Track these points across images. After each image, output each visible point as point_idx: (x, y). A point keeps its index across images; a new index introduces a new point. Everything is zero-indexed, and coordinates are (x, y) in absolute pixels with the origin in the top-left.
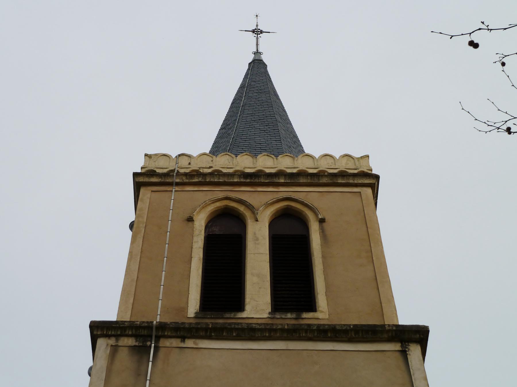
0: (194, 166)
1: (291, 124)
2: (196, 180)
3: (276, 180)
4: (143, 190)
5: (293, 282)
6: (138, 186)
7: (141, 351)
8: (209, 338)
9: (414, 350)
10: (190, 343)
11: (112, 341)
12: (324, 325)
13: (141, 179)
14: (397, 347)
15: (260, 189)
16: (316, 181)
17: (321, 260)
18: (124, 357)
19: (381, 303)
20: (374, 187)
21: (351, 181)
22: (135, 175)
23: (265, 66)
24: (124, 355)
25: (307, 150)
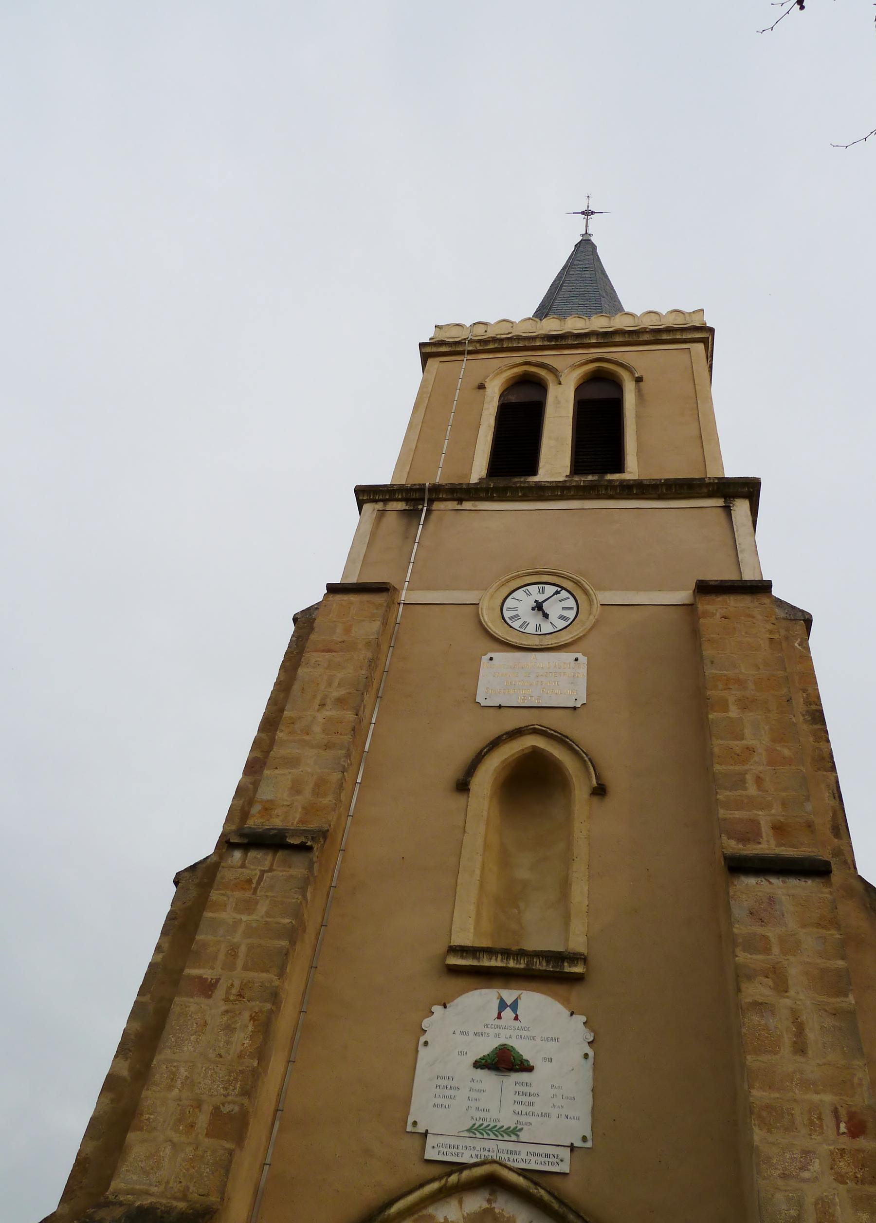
0: (491, 333)
1: (620, 303)
2: (491, 346)
6: (425, 358)
7: (411, 515)
8: (491, 499)
9: (741, 507)
10: (467, 505)
12: (630, 480)
13: (428, 350)
14: (720, 502)
17: (634, 420)
18: (392, 521)
19: (705, 461)
21: (678, 337)
22: (422, 345)
23: (594, 247)
25: (627, 309)
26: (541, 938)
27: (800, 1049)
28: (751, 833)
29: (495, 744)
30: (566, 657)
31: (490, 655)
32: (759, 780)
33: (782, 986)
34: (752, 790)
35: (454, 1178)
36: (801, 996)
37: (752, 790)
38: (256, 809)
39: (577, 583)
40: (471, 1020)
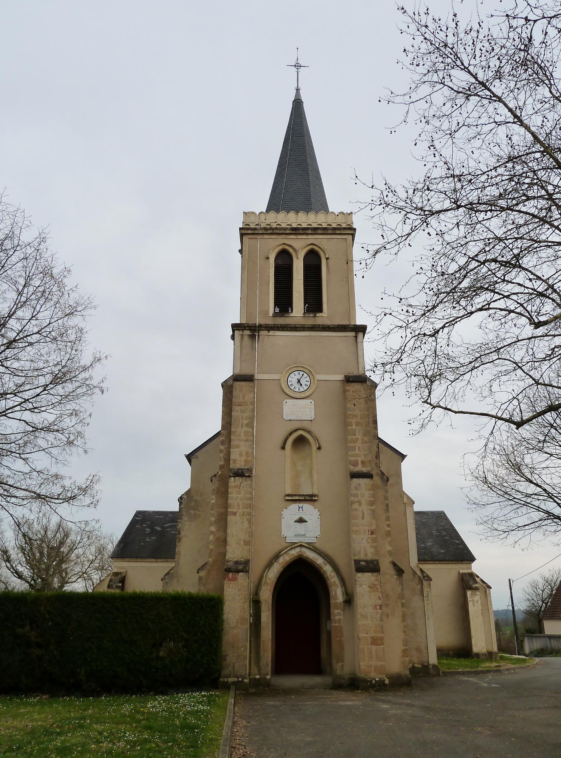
2: (269, 232)
3: (307, 232)
4: (244, 237)
5: (314, 303)
6: (242, 235)
10: (271, 333)
11: (241, 332)
13: (243, 232)
15: (299, 237)
16: (326, 232)
18: (246, 339)
20: (353, 235)
21: (343, 232)
22: (240, 229)
24: (246, 338)
26: (306, 491)
27: (363, 518)
28: (355, 464)
29: (291, 434)
30: (307, 401)
31: (286, 400)
32: (359, 448)
33: (360, 504)
34: (357, 452)
35: (293, 546)
36: (365, 507)
37: (357, 452)
38: (231, 462)
39: (310, 371)
40: (292, 511)
